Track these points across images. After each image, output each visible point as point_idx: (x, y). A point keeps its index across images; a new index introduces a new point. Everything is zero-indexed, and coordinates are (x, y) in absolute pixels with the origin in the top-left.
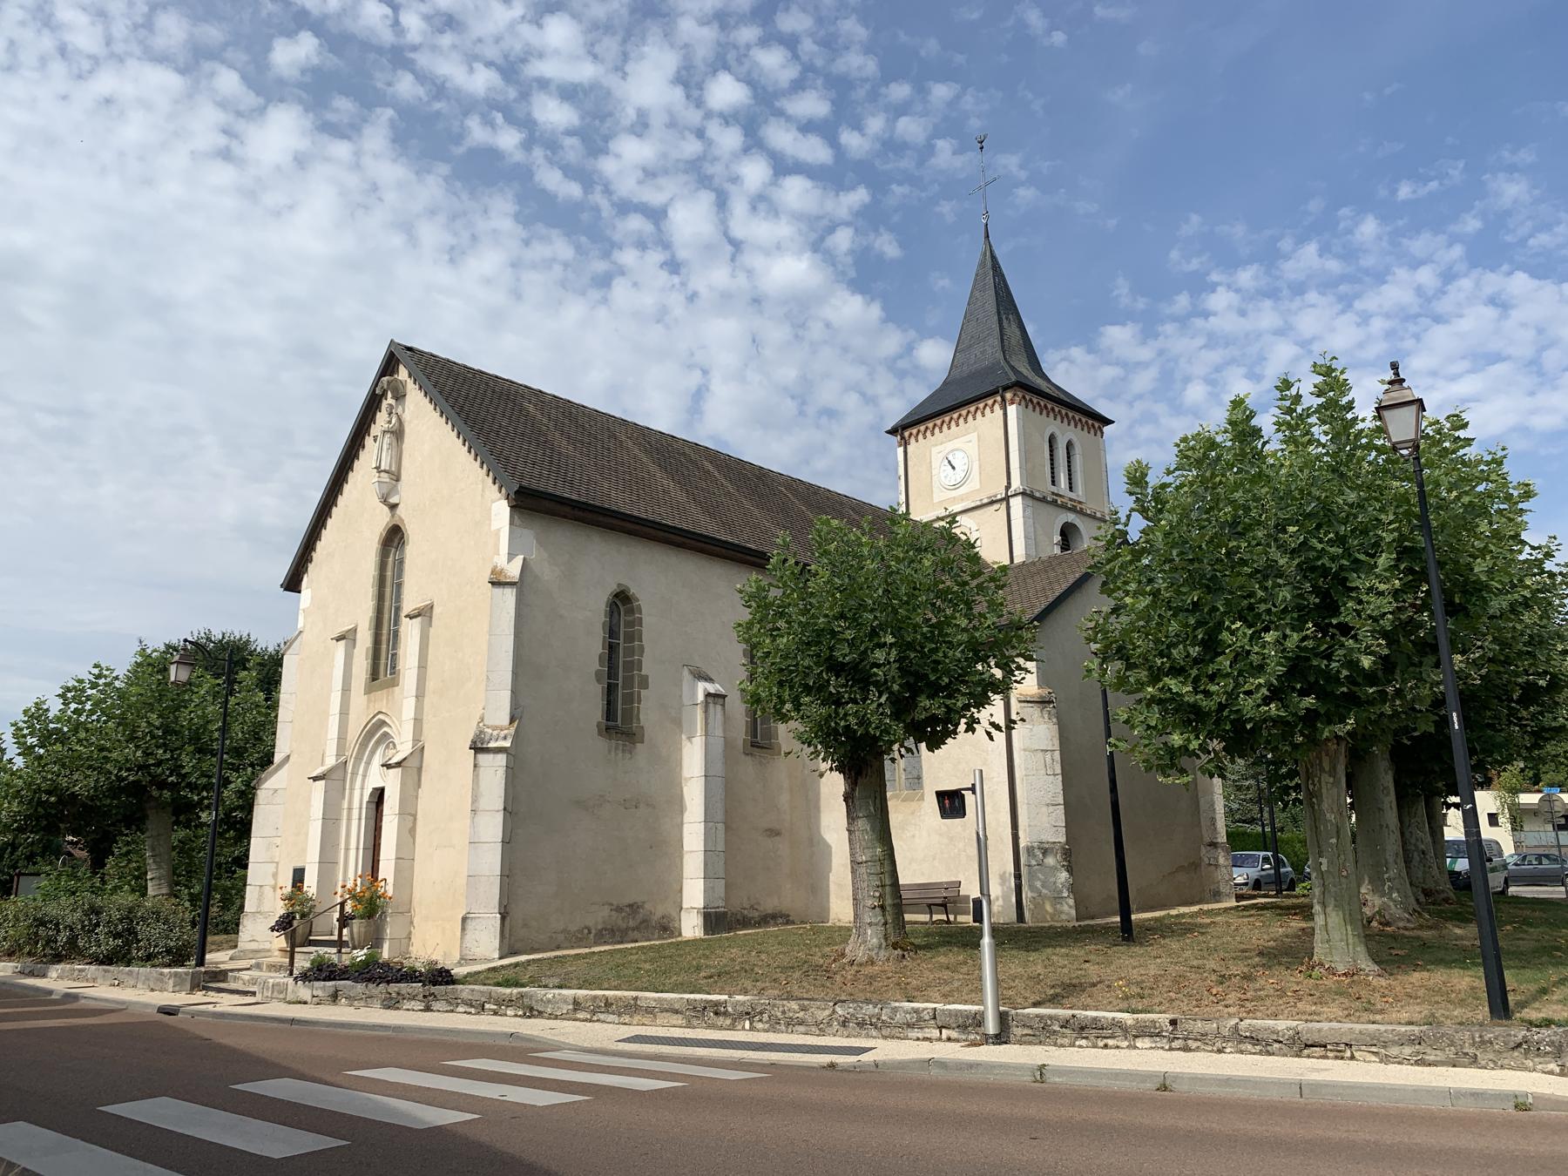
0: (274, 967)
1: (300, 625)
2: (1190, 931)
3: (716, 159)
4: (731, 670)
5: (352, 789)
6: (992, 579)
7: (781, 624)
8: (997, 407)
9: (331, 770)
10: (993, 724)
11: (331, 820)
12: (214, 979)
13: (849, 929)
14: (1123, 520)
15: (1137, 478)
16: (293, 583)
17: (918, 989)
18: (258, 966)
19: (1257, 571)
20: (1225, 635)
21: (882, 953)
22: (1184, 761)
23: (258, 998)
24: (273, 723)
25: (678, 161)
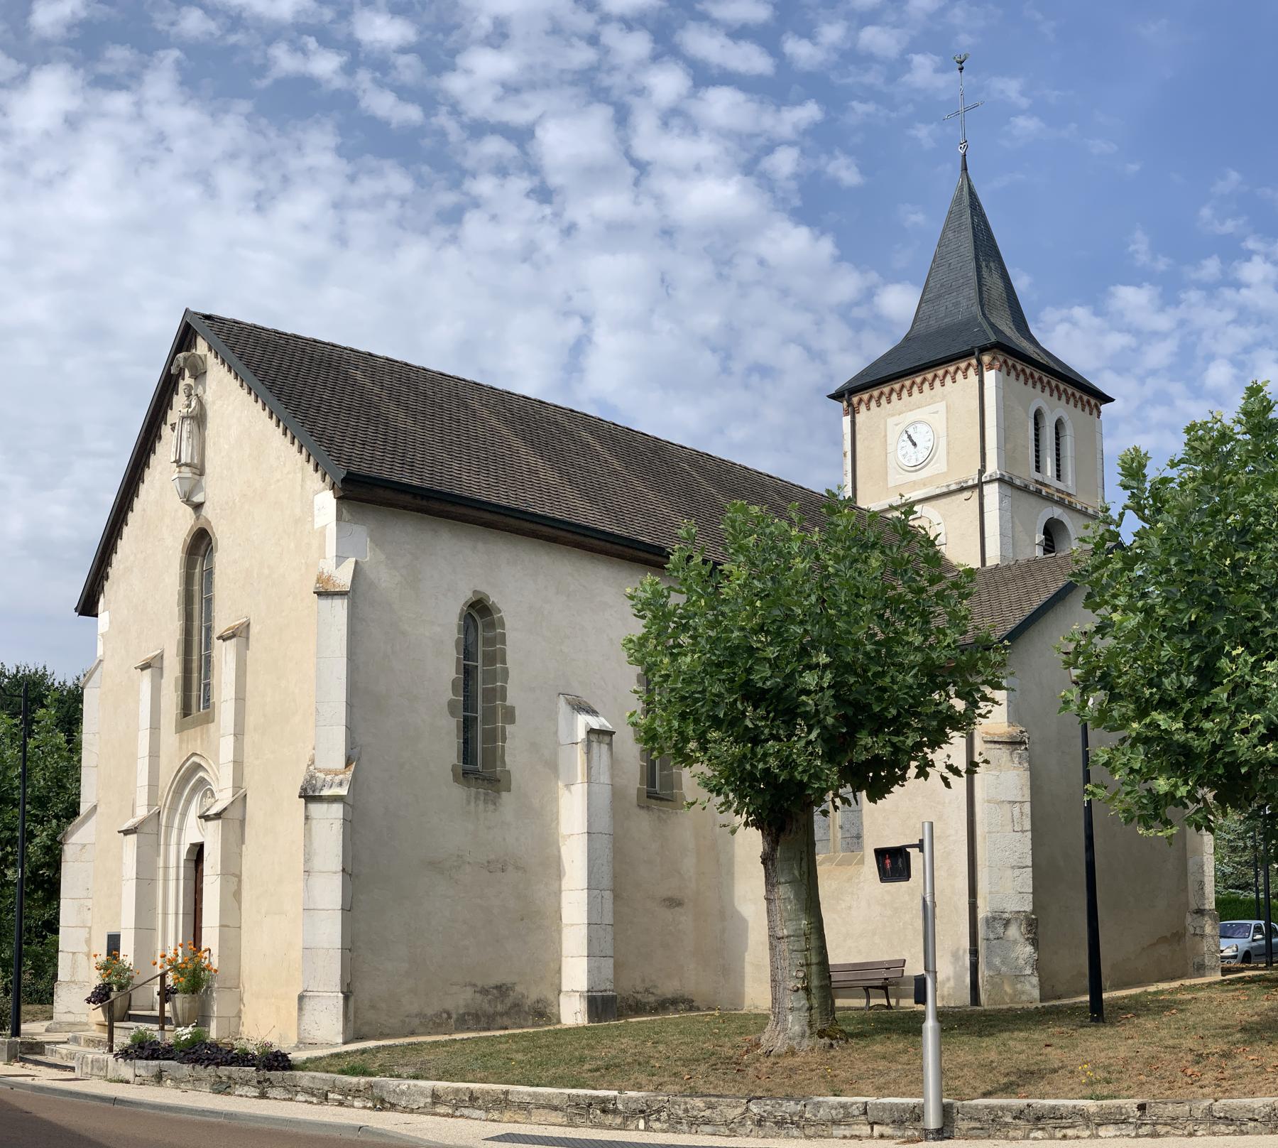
0: (91, 1042)
1: (100, 652)
2: (1169, 1008)
3: (613, 69)
4: (620, 696)
5: (167, 845)
6: (955, 586)
7: (684, 639)
8: (971, 372)
9: (143, 822)
10: (950, 768)
11: (145, 880)
12: (30, 1051)
13: (766, 1017)
14: (1116, 517)
15: (1133, 469)
16: (88, 606)
17: (848, 1082)
18: (76, 1040)
19: (1264, 588)
20: (1224, 663)
21: (806, 1042)
22: (1170, 811)
23: (77, 1074)
24: (77, 767)
25: (562, 71)
